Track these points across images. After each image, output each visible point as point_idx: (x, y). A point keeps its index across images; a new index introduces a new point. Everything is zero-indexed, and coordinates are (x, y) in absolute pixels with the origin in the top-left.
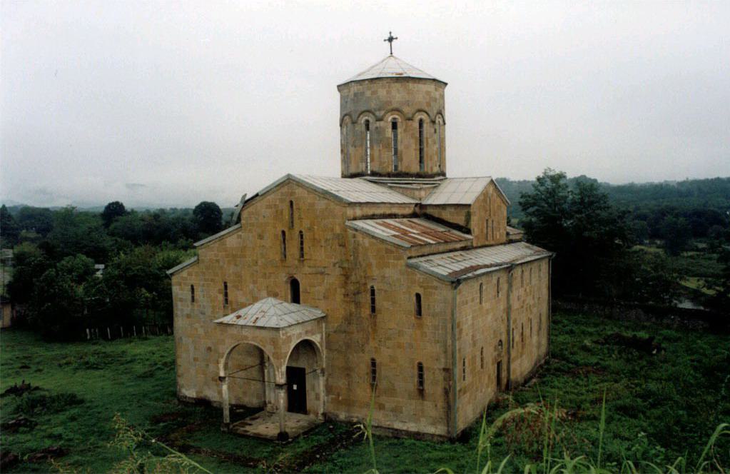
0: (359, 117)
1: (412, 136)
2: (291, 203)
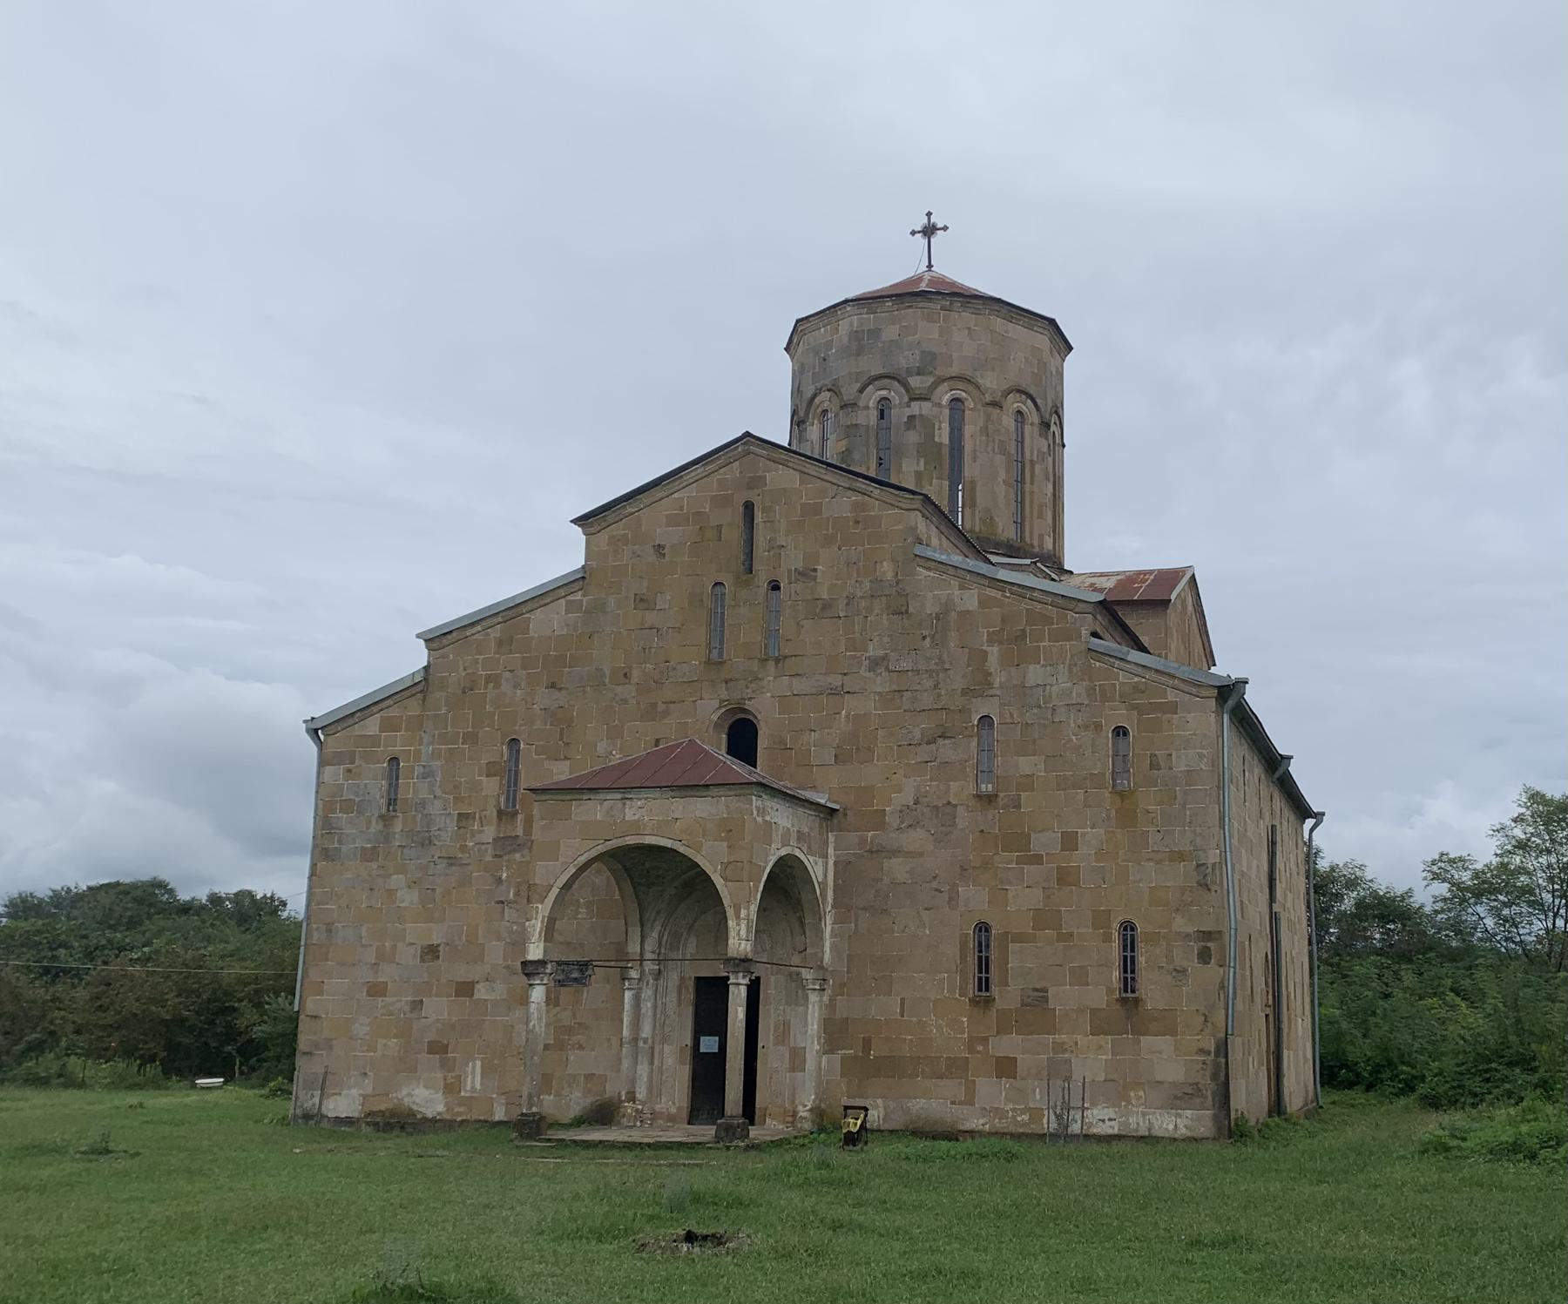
0: (861, 391)
1: (1003, 450)
2: (749, 508)
